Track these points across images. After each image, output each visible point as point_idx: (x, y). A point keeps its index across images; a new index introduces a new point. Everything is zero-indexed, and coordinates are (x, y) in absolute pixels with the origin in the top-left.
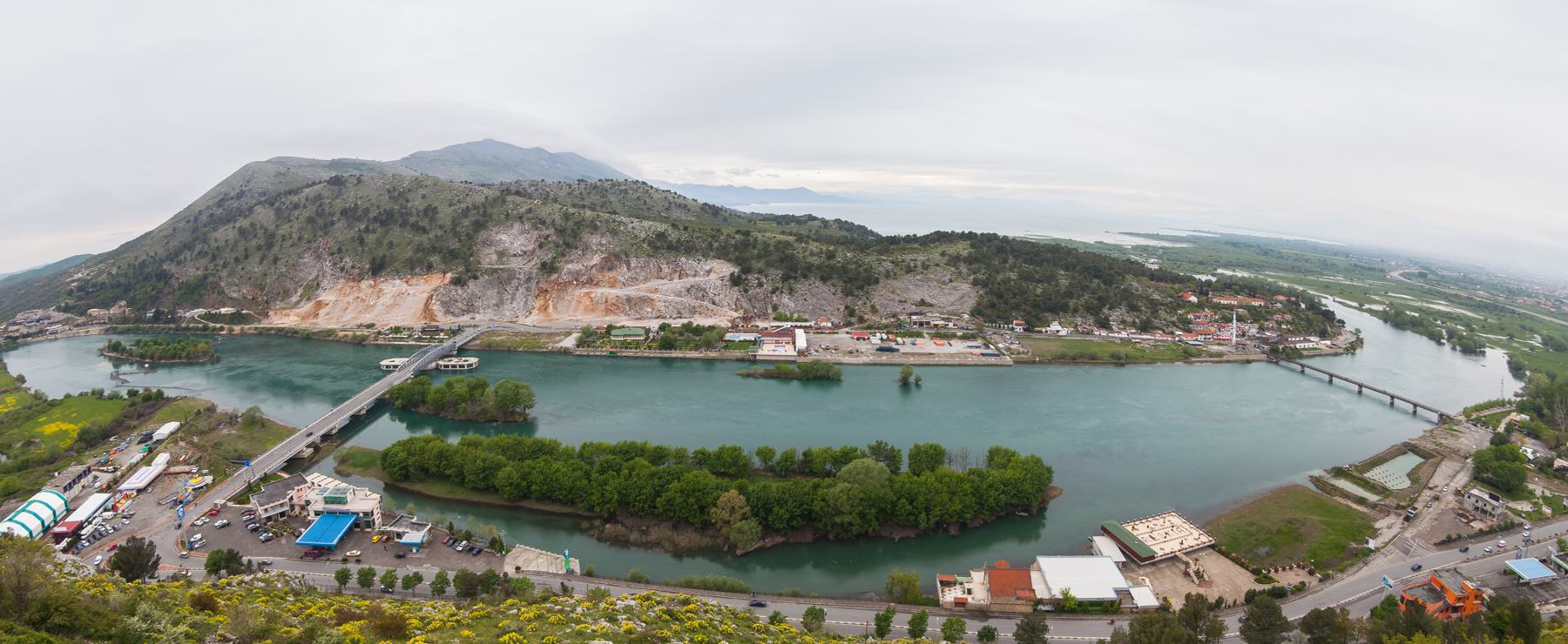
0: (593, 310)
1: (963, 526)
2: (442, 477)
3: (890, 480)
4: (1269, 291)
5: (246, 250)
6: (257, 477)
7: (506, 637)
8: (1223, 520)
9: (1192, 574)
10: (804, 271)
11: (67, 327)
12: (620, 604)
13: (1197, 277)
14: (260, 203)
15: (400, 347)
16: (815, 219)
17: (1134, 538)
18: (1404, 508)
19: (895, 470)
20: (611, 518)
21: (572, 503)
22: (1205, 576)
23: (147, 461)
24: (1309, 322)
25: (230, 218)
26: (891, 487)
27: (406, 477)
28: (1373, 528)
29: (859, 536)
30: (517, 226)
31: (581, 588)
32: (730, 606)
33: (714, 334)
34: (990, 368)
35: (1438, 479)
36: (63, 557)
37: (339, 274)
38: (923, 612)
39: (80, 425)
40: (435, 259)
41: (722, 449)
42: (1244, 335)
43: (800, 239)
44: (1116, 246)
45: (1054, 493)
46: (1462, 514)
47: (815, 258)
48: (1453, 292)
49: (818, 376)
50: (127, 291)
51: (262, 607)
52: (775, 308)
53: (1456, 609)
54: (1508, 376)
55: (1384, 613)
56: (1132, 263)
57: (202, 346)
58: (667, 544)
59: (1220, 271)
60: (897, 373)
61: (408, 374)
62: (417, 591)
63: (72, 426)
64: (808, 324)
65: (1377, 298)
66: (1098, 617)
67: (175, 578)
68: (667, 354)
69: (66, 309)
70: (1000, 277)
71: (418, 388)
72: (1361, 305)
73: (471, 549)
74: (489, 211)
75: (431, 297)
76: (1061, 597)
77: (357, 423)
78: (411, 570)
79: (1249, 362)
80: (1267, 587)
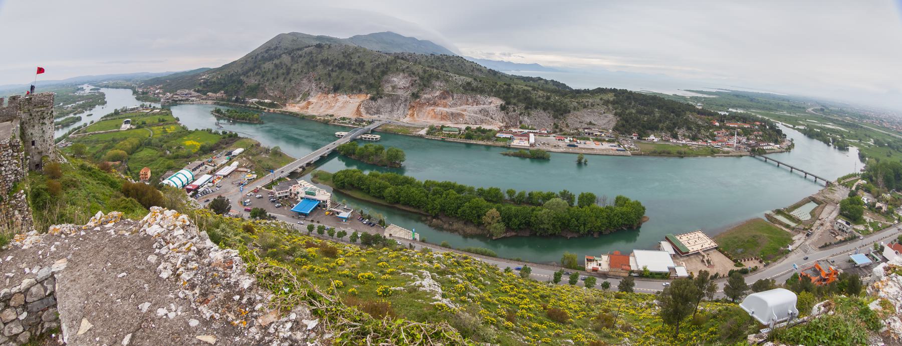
0: (435, 118)
1: (601, 233)
2: (359, 189)
3: (568, 209)
4: (753, 120)
5: (277, 74)
6: (276, 178)
7: (381, 264)
8: (723, 235)
9: (705, 261)
10: (536, 105)
11: (198, 99)
12: (435, 256)
13: (720, 113)
14: (284, 53)
15: (345, 127)
16: (542, 79)
17: (680, 243)
18: (807, 229)
19: (571, 205)
20: (436, 217)
21: (419, 207)
22: (711, 263)
23: (229, 163)
24: (770, 135)
25: (271, 59)
26: (569, 212)
27: (343, 187)
28: (792, 240)
29: (551, 235)
30: (401, 74)
31: (418, 247)
32: (486, 262)
33: (491, 133)
34: (621, 157)
35: (823, 215)
36: (190, 199)
37: (318, 90)
38: (577, 273)
39: (201, 143)
40: (363, 87)
41: (491, 189)
42: (740, 143)
43: (534, 89)
44: (683, 97)
45: (645, 220)
46: (833, 232)
47: (541, 99)
48: (836, 118)
49: (539, 157)
50: (224, 87)
51: (274, 235)
52: (521, 122)
53: (825, 280)
54: (859, 160)
55: (792, 282)
56: (690, 105)
57: (256, 116)
58: (461, 231)
59: (730, 110)
60: (576, 157)
61: (348, 140)
62: (343, 239)
63: (197, 143)
64: (536, 131)
65: (801, 122)
66: (659, 280)
67: (237, 217)
68: (468, 141)
69: (198, 91)
70: (627, 112)
71: (351, 147)
72: (794, 126)
73: (370, 224)
74: (389, 66)
75: (360, 105)
76: (643, 270)
77: (323, 160)
78: (342, 229)
79: (741, 156)
80: (739, 268)
